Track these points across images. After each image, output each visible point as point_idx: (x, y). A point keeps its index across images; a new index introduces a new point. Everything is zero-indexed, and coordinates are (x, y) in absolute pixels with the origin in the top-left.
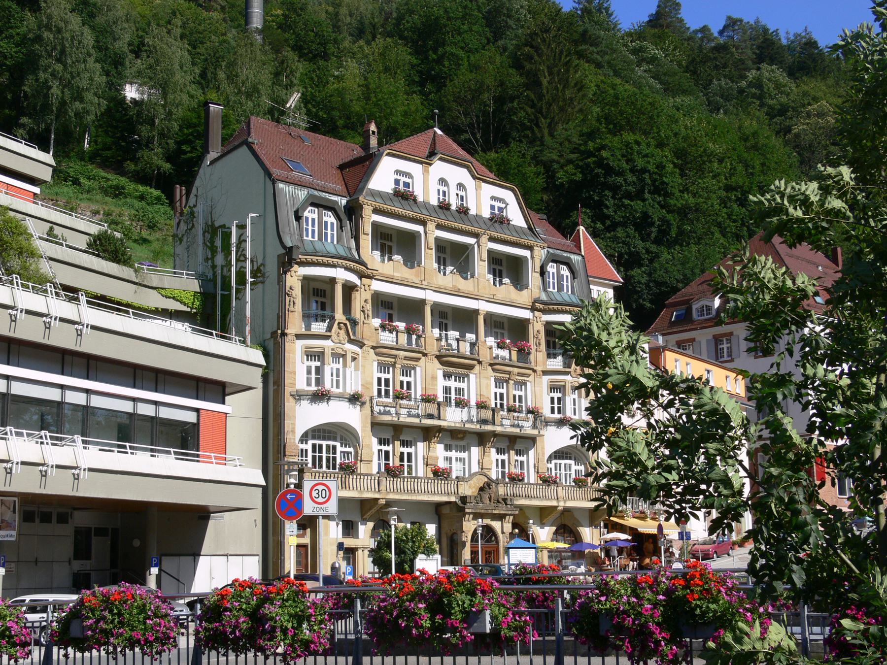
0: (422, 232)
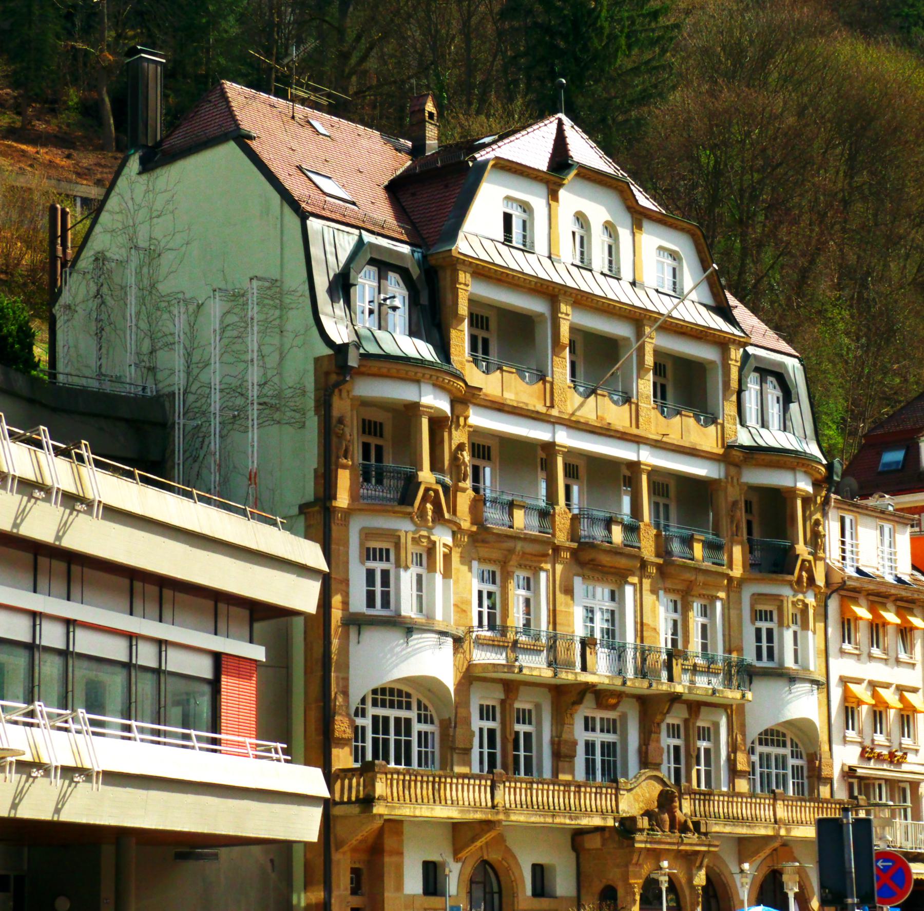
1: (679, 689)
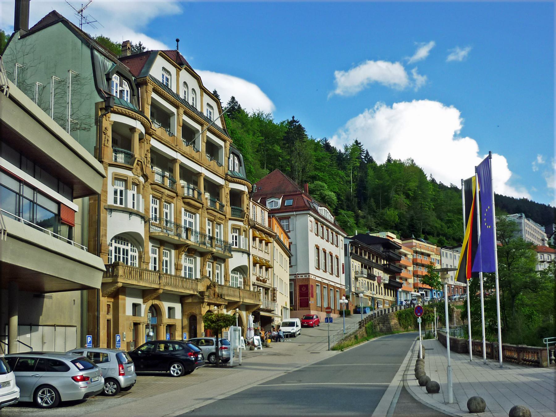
0: (176, 113)
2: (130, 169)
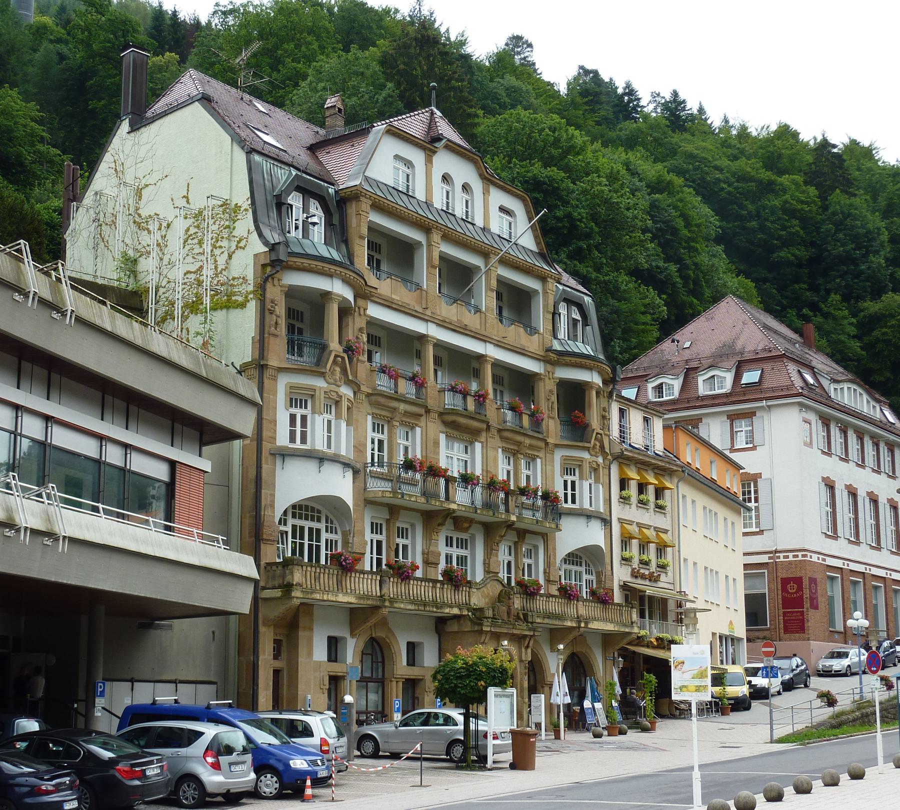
1: (513, 518)
2: (322, 375)
